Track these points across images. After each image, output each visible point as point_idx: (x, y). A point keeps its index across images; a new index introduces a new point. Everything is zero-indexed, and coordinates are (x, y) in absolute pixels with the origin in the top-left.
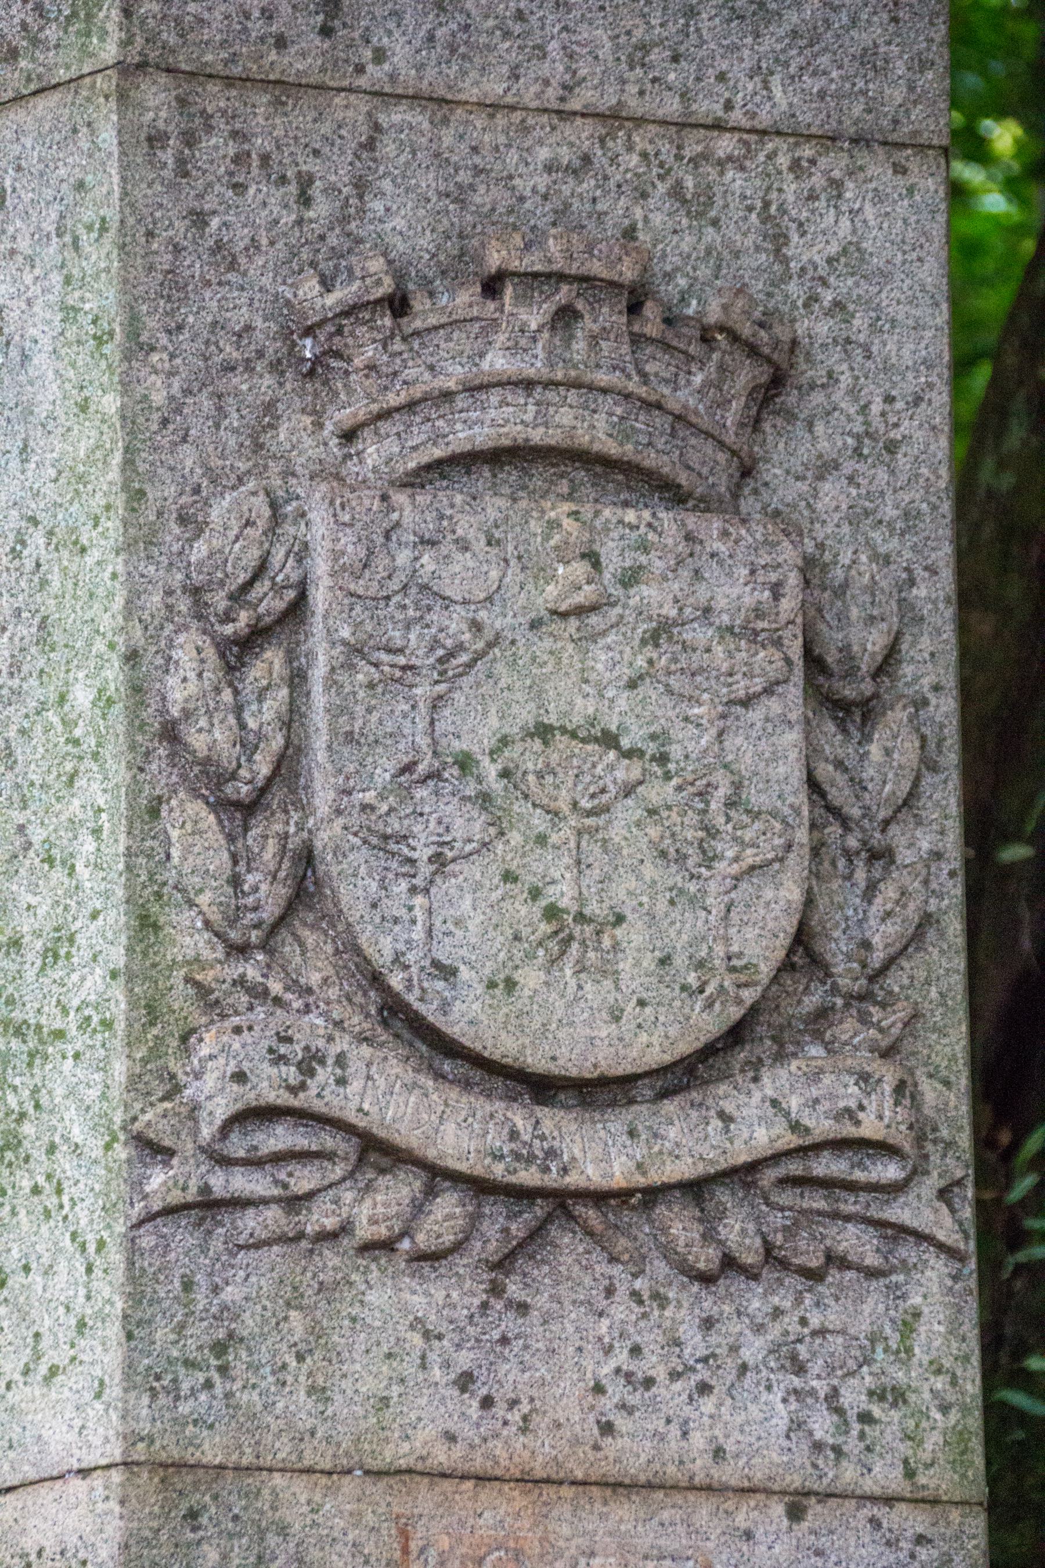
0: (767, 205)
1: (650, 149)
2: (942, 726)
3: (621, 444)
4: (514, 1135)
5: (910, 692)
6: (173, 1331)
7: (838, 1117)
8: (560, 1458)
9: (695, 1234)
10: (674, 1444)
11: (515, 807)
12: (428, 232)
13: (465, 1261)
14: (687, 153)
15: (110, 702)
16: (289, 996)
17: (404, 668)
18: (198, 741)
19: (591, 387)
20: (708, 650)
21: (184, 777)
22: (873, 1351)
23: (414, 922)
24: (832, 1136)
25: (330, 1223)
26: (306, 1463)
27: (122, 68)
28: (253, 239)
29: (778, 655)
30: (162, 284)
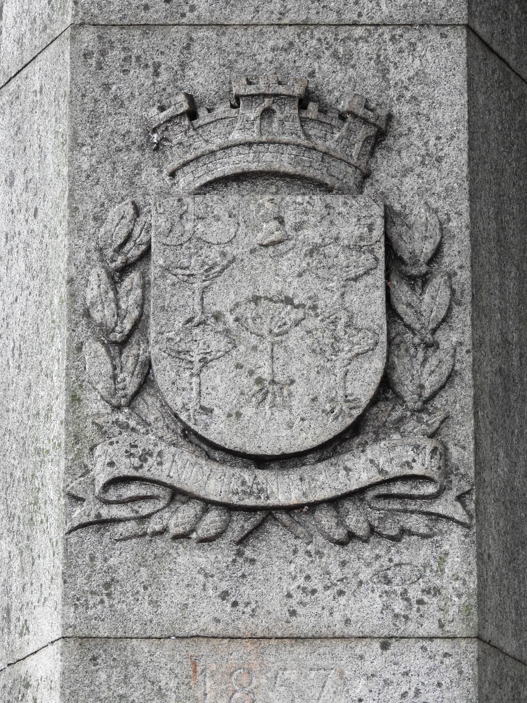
0: (379, 56)
1: (322, 37)
2: (463, 284)
3: (295, 167)
4: (244, 483)
5: (448, 270)
6: (85, 579)
7: (402, 466)
8: (270, 627)
9: (333, 522)
10: (326, 618)
11: (242, 334)
12: (214, 83)
13: (225, 541)
14: (340, 37)
15: (63, 302)
16: (139, 427)
17: (189, 276)
18: (97, 316)
19: (280, 143)
20: (337, 257)
21: (93, 333)
22: (425, 572)
23: (192, 389)
24: (398, 474)
25: (158, 528)
26: (148, 634)
27: (74, 26)
28: (132, 93)
29: (371, 257)
30: (88, 117)
